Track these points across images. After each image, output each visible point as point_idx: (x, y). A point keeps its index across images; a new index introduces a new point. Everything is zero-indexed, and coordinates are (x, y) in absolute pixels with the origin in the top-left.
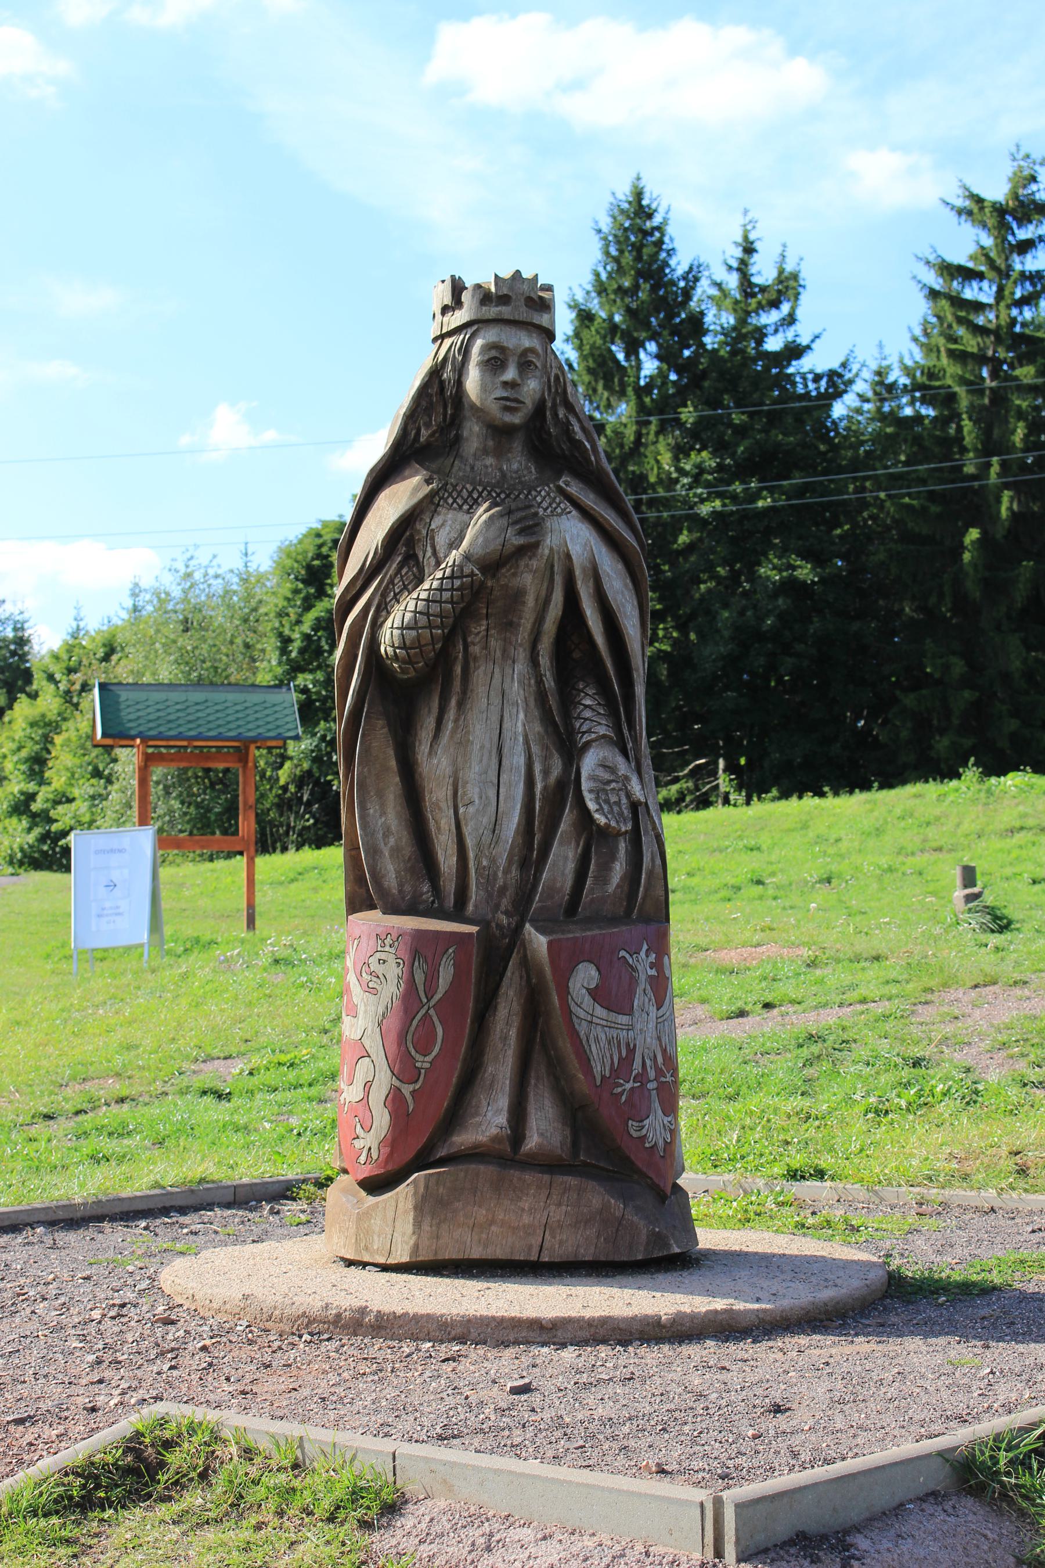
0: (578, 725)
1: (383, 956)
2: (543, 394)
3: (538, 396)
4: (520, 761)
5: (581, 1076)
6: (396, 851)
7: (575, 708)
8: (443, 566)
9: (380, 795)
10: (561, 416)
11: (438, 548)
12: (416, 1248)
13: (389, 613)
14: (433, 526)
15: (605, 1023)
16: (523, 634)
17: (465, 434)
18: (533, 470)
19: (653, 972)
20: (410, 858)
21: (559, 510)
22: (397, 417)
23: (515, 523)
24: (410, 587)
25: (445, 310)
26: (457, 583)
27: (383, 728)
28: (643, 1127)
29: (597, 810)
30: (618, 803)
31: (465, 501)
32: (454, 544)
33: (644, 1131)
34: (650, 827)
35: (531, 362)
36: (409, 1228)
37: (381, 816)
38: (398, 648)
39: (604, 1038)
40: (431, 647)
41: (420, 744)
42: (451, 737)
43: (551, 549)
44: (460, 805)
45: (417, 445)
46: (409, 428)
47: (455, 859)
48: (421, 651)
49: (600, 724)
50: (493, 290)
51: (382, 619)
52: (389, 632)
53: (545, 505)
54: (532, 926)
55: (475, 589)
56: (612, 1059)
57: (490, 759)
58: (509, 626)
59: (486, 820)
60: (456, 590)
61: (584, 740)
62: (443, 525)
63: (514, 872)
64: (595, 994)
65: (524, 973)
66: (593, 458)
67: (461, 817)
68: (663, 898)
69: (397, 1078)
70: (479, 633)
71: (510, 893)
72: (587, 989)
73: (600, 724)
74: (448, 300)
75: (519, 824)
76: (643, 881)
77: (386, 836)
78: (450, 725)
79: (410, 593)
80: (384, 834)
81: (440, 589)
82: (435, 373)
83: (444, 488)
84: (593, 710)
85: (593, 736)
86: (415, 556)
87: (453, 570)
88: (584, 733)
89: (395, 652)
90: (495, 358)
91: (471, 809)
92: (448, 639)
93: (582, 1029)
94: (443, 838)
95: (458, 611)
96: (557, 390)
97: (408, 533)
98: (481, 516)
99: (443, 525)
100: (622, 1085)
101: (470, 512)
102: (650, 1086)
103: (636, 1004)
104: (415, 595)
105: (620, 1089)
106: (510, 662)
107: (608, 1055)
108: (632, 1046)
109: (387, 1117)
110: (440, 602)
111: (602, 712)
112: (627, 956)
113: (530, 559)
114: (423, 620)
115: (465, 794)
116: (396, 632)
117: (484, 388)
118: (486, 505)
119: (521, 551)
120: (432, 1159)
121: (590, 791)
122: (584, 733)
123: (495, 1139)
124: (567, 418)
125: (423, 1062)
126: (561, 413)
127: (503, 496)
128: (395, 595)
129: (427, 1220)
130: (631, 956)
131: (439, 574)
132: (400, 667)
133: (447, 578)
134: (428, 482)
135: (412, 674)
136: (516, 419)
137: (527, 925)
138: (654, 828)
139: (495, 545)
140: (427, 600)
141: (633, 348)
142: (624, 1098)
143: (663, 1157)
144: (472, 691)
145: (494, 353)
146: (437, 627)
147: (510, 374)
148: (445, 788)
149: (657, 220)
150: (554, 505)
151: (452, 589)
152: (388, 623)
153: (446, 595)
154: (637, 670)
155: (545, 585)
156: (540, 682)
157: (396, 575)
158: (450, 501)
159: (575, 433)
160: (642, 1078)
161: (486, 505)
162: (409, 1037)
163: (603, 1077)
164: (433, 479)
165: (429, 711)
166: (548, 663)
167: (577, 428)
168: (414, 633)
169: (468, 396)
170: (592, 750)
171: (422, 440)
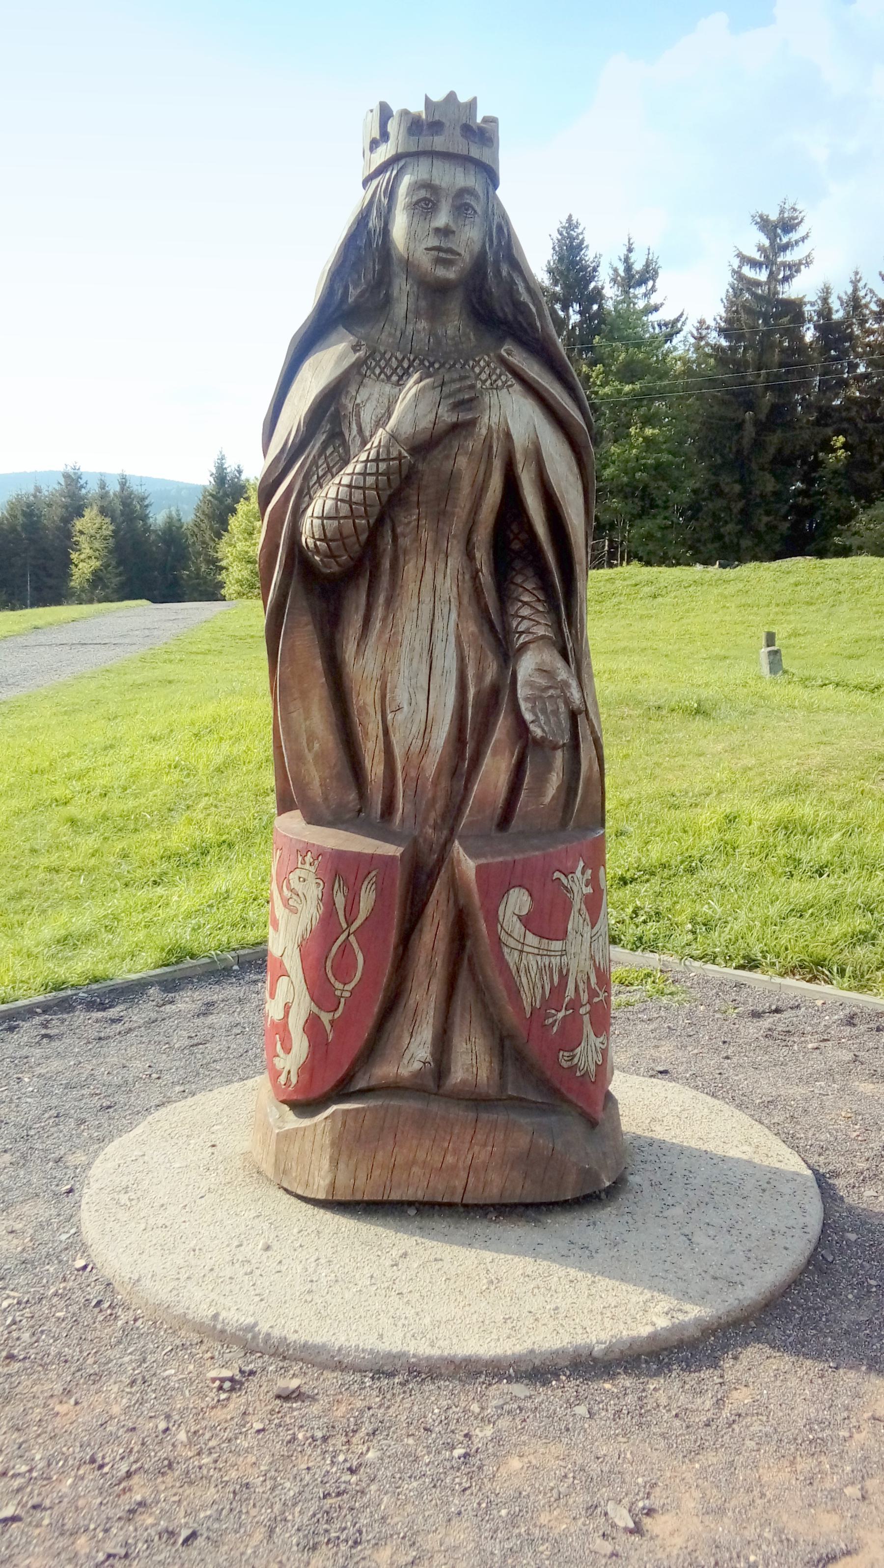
0: (514, 624)
1: (303, 874)
2: (484, 245)
3: (477, 248)
4: (451, 663)
5: (510, 1008)
6: (320, 757)
7: (512, 604)
8: (368, 446)
9: (304, 695)
10: (504, 273)
11: (363, 426)
12: (333, 1185)
13: (311, 499)
14: (358, 401)
15: (536, 951)
16: (457, 525)
17: (396, 293)
18: (472, 337)
19: (589, 890)
20: (335, 765)
21: (500, 383)
22: (323, 273)
23: (449, 396)
24: (334, 470)
25: (374, 144)
26: (383, 466)
27: (306, 625)
28: (574, 1056)
29: (532, 722)
30: (556, 713)
31: (395, 371)
32: (381, 422)
33: (576, 1060)
34: (589, 732)
35: (466, 204)
36: (326, 1164)
37: (305, 720)
38: (320, 540)
39: (535, 967)
40: (354, 539)
41: (347, 643)
42: (379, 638)
43: (490, 428)
44: (388, 711)
45: (345, 307)
46: (336, 287)
47: (382, 767)
48: (344, 544)
49: (538, 623)
50: (424, 116)
51: (304, 506)
52: (309, 521)
53: (484, 376)
54: (460, 844)
55: (404, 473)
56: (543, 987)
57: (420, 662)
58: (441, 515)
59: (417, 727)
60: (381, 474)
61: (521, 641)
62: (369, 398)
63: (444, 783)
64: (527, 921)
65: (451, 895)
66: (538, 324)
67: (389, 723)
68: (600, 804)
69: (316, 1004)
70: (409, 523)
71: (440, 805)
72: (519, 917)
73: (538, 623)
74: (376, 134)
75: (449, 733)
76: (580, 791)
77: (310, 742)
78: (378, 625)
79: (333, 477)
80: (308, 739)
81: (364, 474)
82: (362, 220)
83: (371, 356)
84: (531, 607)
85: (531, 637)
86: (341, 434)
87: (378, 452)
88: (522, 633)
89: (315, 545)
90: (424, 199)
91: (400, 716)
92: (375, 531)
93: (512, 958)
94: (370, 745)
95: (384, 499)
96: (500, 242)
97: (333, 408)
98: (410, 389)
99: (369, 398)
100: (555, 1015)
101: (399, 384)
102: (582, 1011)
103: (570, 927)
104: (336, 480)
105: (551, 1020)
106: (442, 556)
107: (539, 986)
108: (564, 972)
109: (306, 1043)
110: (363, 488)
111: (541, 609)
112: (562, 877)
113: (466, 439)
114: (344, 509)
115: (393, 699)
116: (317, 522)
117: (412, 235)
118: (416, 376)
119: (455, 428)
120: (352, 1090)
121: (527, 699)
122: (522, 633)
123: (418, 1074)
124: (512, 277)
125: (343, 990)
126: (505, 270)
127: (437, 366)
128: (319, 478)
129: (344, 1158)
130: (566, 876)
131: (363, 457)
132: (321, 560)
133: (372, 461)
134: (355, 348)
135: (335, 568)
136: (450, 274)
137: (456, 843)
138: (593, 732)
139: (425, 423)
140: (349, 486)
141: (565, 308)
142: (555, 1029)
143: (593, 1083)
144: (402, 587)
145: (423, 193)
146: (361, 517)
147: (442, 219)
148: (372, 691)
149: (579, 231)
150: (494, 377)
151: (377, 474)
152: (309, 512)
153: (370, 480)
154: (581, 564)
155: (482, 468)
156: (475, 577)
157: (320, 455)
158: (377, 371)
159: (520, 294)
160: (575, 1004)
161: (416, 376)
162: (329, 964)
163: (533, 1009)
164: (360, 346)
165: (357, 607)
166: (485, 557)
167: (521, 289)
168: (335, 523)
169: (396, 248)
170: (529, 653)
171: (350, 300)
